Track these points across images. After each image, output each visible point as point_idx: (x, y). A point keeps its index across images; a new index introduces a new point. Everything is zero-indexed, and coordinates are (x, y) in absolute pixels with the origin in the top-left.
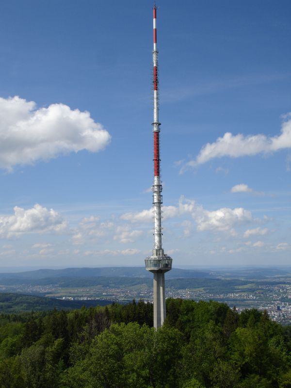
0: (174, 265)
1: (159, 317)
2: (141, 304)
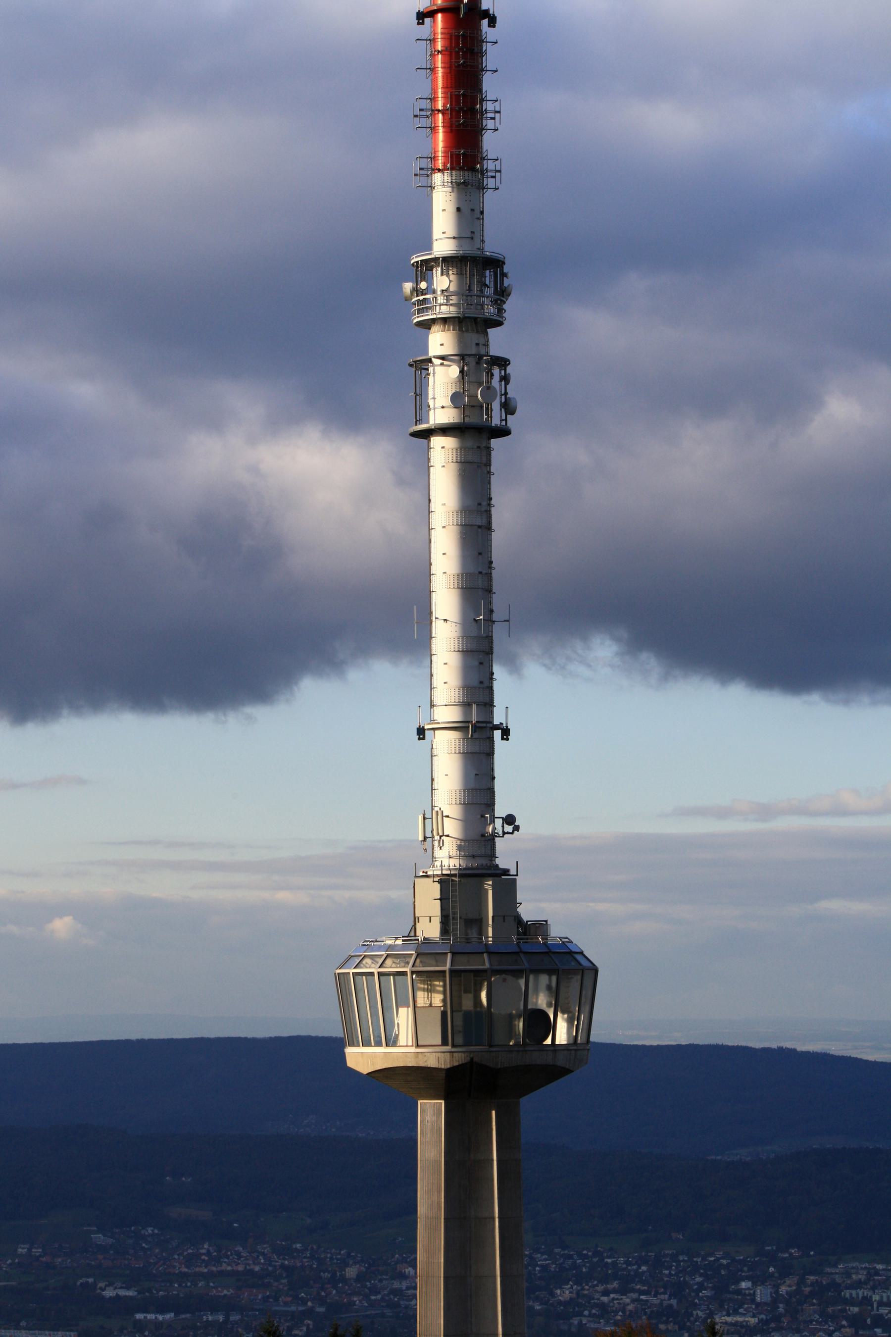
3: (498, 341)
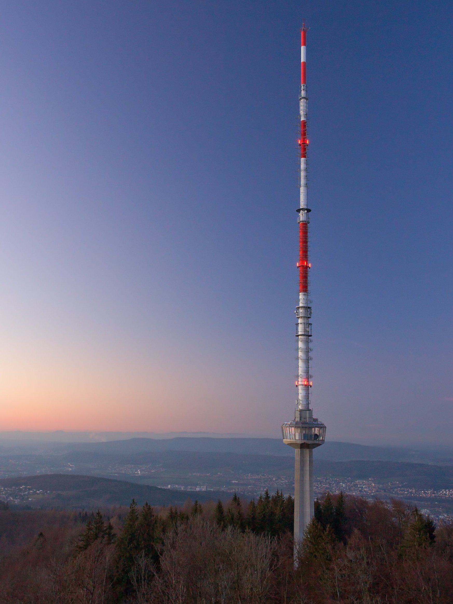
0: (330, 436)
1: (303, 518)
2: (278, 499)
3: (310, 321)
